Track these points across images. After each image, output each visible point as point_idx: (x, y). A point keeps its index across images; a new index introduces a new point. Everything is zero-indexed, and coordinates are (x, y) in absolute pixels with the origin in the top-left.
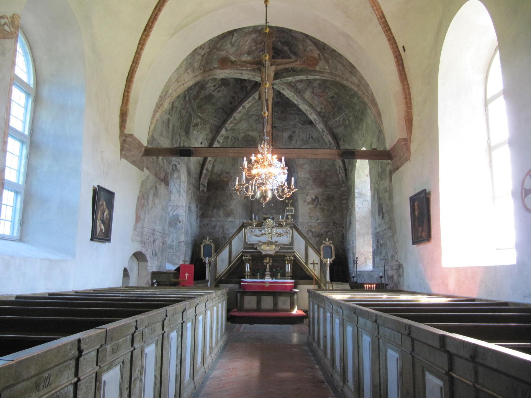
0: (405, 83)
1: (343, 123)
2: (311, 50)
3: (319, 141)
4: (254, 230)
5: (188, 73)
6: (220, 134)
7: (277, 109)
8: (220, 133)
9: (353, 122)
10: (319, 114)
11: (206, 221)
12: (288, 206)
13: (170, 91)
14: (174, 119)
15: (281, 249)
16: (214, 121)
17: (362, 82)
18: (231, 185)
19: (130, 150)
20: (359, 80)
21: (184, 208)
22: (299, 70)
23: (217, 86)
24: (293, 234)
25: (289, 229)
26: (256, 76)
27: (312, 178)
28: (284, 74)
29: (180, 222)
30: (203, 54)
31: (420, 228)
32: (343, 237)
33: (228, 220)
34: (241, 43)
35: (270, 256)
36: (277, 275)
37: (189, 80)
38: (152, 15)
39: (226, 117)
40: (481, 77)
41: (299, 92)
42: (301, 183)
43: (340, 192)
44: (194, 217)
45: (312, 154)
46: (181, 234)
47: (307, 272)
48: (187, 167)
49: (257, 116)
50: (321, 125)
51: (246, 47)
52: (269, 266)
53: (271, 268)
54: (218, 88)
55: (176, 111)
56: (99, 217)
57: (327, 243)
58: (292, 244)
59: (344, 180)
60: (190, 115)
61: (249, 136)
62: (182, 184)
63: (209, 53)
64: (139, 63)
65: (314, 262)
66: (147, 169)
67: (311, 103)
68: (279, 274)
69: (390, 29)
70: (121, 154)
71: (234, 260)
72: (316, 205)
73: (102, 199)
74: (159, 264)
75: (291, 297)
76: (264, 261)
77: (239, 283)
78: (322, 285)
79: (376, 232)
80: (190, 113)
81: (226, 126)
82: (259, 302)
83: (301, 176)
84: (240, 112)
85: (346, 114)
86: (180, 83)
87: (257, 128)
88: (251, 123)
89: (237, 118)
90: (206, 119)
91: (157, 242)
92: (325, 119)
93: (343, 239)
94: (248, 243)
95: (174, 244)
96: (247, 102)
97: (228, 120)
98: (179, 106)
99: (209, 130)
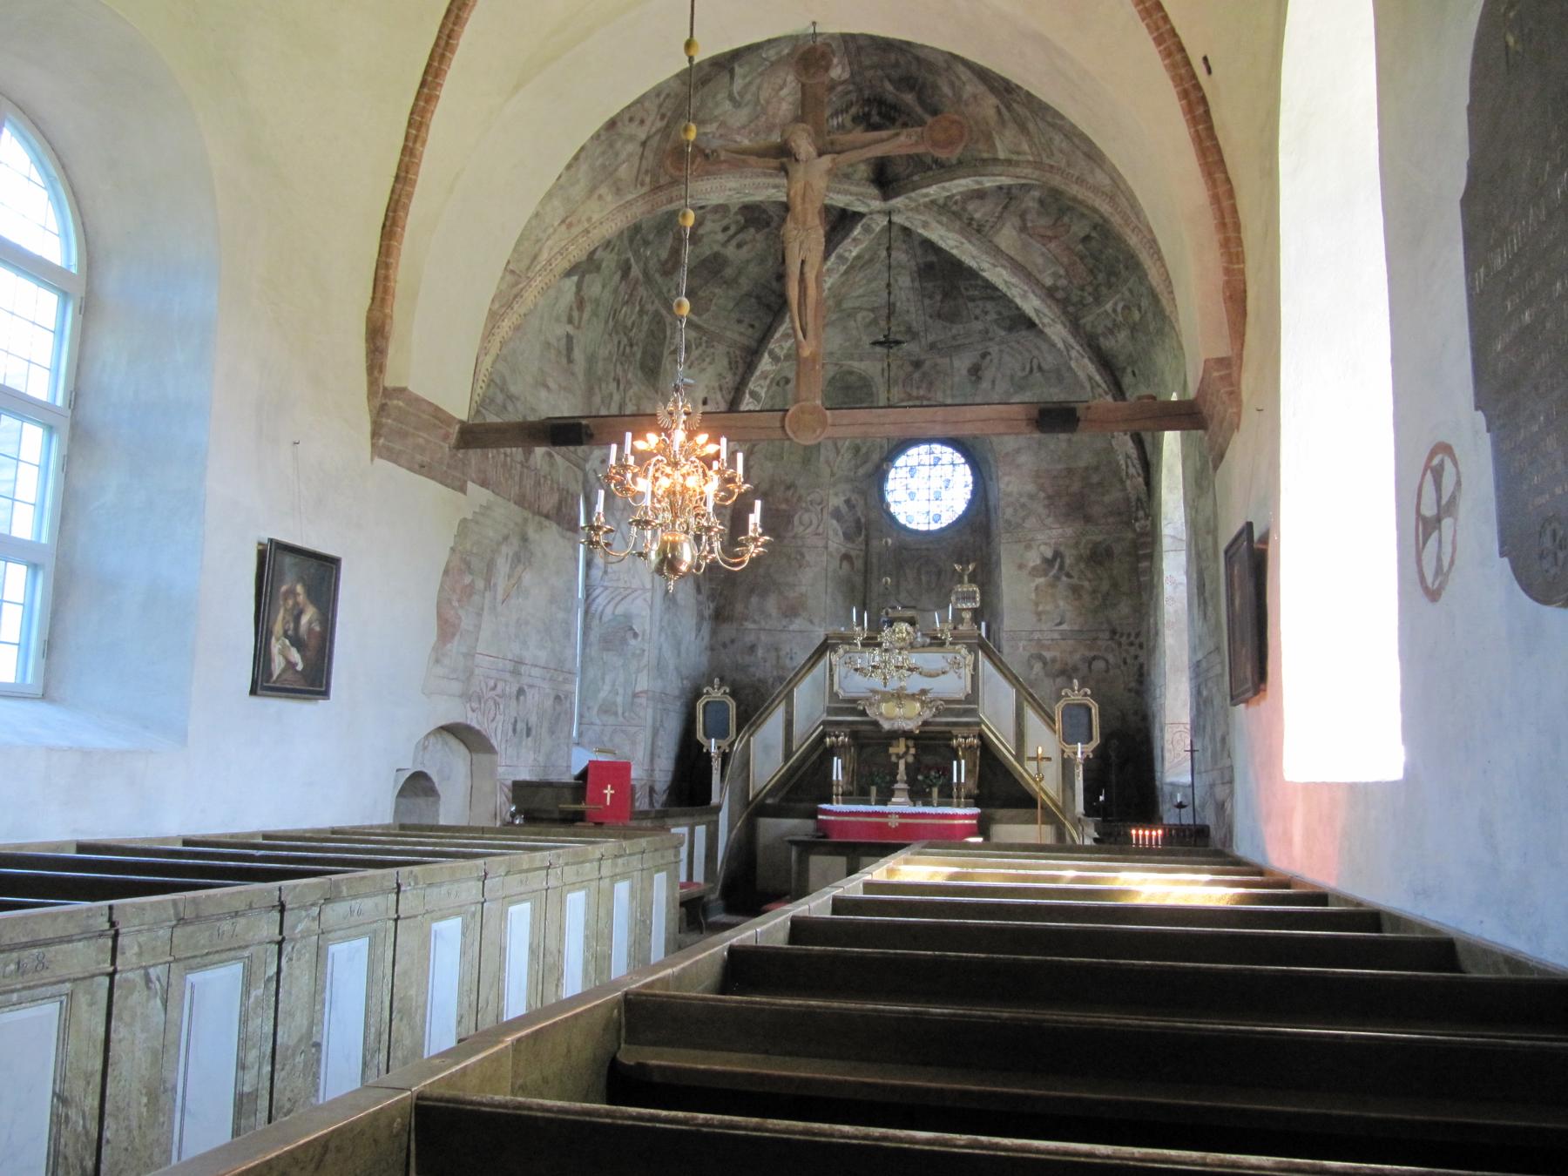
0: (1219, 176)
1: (1125, 318)
2: (975, 97)
3: (1060, 379)
6: (757, 373)
7: (930, 285)
9: (1150, 315)
10: (1050, 293)
11: (728, 631)
12: (961, 582)
13: (545, 256)
14: (592, 337)
15: (939, 713)
16: (737, 334)
18: (801, 523)
19: (404, 435)
21: (648, 595)
22: (954, 161)
24: (975, 668)
25: (964, 651)
27: (1042, 495)
28: (916, 178)
29: (635, 635)
30: (643, 137)
33: (791, 628)
34: (764, 95)
35: (908, 735)
36: (930, 794)
37: (606, 217)
38: (439, 38)
39: (769, 320)
41: (979, 231)
42: (1009, 511)
43: (1130, 535)
45: (945, 422)
46: (638, 671)
49: (873, 310)
50: (1059, 327)
51: (784, 106)
52: (907, 765)
54: (736, 234)
55: (595, 314)
56: (278, 628)
57: (1077, 694)
58: (973, 697)
59: (1144, 497)
61: (851, 373)
65: (1048, 757)
66: (484, 484)
67: (1019, 258)
68: (935, 791)
71: (800, 747)
72: (1057, 578)
74: (541, 759)
76: (892, 750)
77: (812, 814)
81: (771, 346)
83: (1009, 489)
85: (1131, 291)
86: (576, 230)
88: (854, 332)
91: (532, 697)
92: (1071, 309)
93: (1141, 682)
94: (842, 694)
95: (619, 699)
98: (607, 296)
99: (725, 362)
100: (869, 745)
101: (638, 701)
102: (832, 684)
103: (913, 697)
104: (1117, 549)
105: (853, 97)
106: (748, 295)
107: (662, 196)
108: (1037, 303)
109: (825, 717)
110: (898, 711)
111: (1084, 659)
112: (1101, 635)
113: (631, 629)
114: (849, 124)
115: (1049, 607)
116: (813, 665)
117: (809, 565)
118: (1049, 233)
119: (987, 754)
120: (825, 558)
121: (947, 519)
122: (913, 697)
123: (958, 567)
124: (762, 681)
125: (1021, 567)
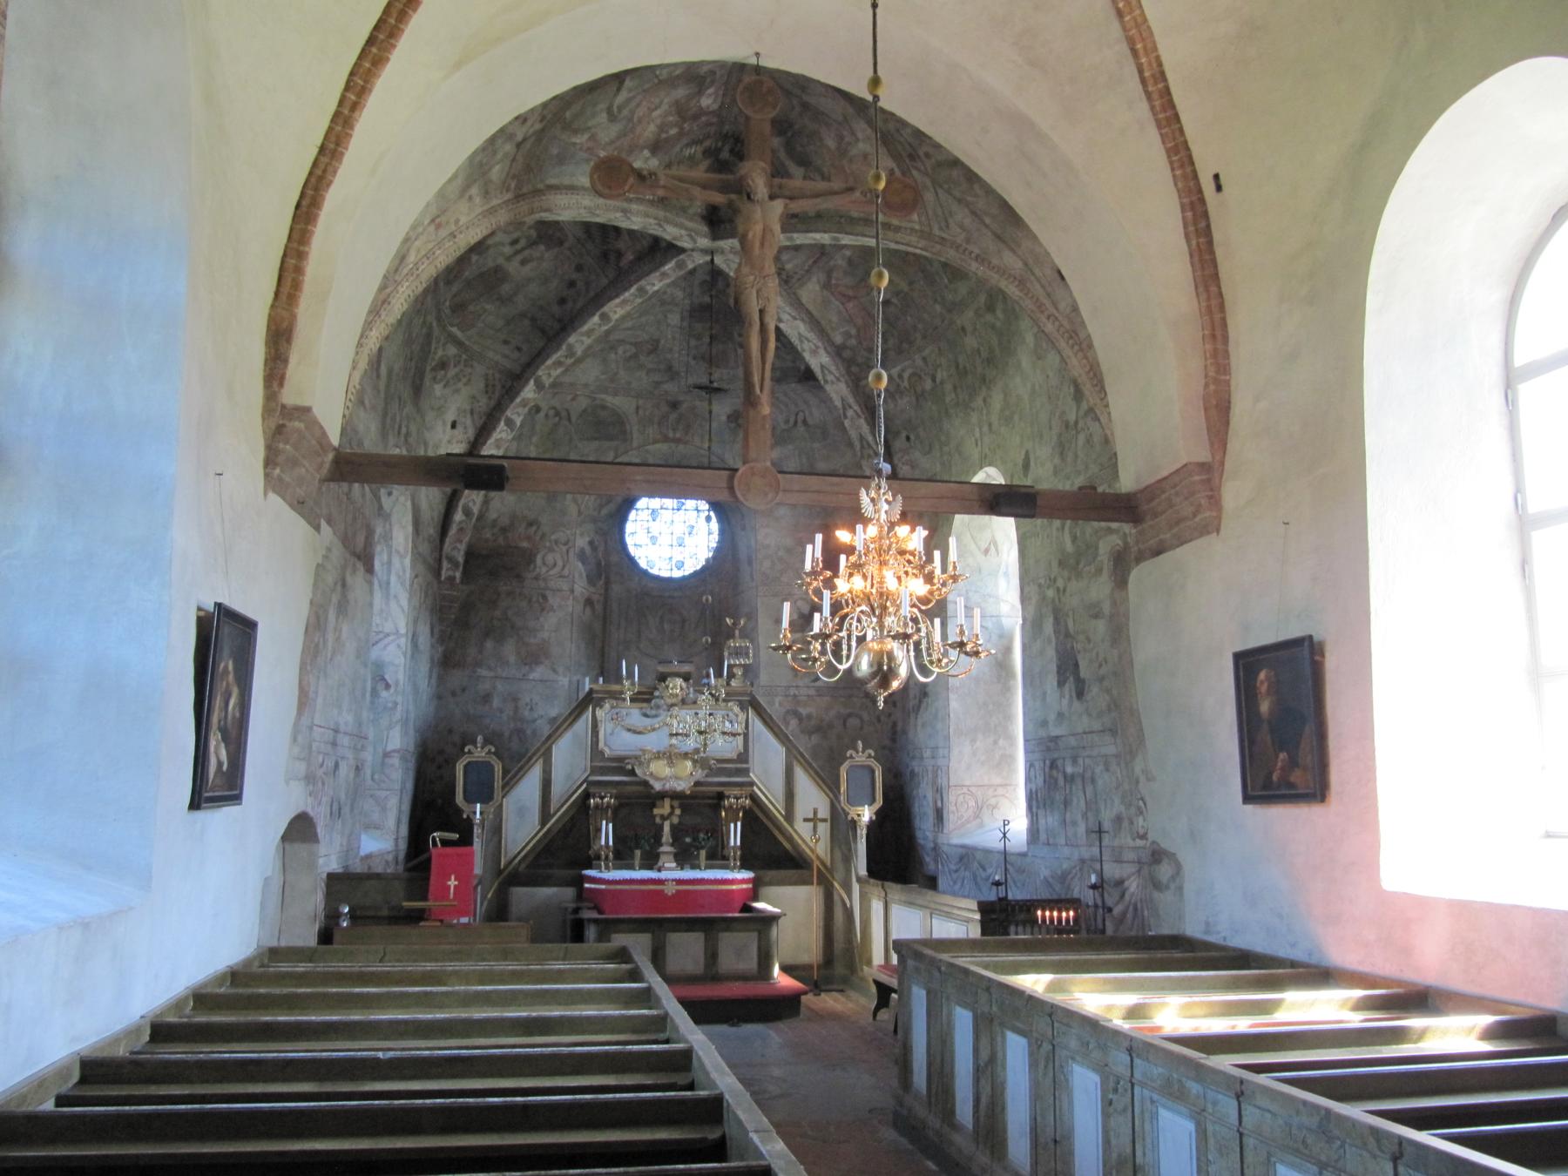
0: (1213, 289)
4: (624, 712)
5: (470, 198)
6: (518, 400)
7: (698, 326)
8: (518, 393)
9: (948, 387)
10: (838, 351)
11: (457, 678)
12: (733, 636)
13: (412, 258)
16: (500, 356)
17: (1037, 271)
20: (1026, 264)
21: (403, 640)
23: (523, 243)
25: (736, 709)
26: (668, 221)
29: (388, 686)
30: (519, 137)
31: (1283, 756)
34: (640, 112)
35: (675, 796)
36: (697, 857)
37: (471, 224)
39: (541, 344)
40: (1495, 297)
41: (786, 282)
42: (767, 564)
44: (424, 667)
46: (390, 727)
47: (787, 845)
48: (413, 504)
49: (635, 344)
52: (672, 826)
56: (215, 719)
58: (743, 757)
60: (429, 335)
61: (604, 407)
62: (396, 561)
63: (540, 135)
64: (342, 154)
66: (329, 522)
68: (703, 853)
69: (1177, 117)
70: (266, 475)
71: (559, 813)
73: (226, 652)
76: (656, 811)
79: (1042, 733)
80: (430, 327)
81: (540, 373)
84: (589, 333)
85: (924, 359)
86: (443, 233)
87: (629, 383)
88: (613, 366)
89: (579, 351)
90: (475, 347)
91: (344, 769)
93: (894, 740)
94: (607, 752)
96: (617, 301)
97: (548, 356)
99: (482, 385)
101: (389, 761)
103: (686, 756)
105: (713, 129)
106: (523, 315)
107: (524, 206)
108: (825, 359)
110: (667, 771)
113: (383, 679)
114: (699, 155)
116: (575, 720)
117: (552, 609)
118: (851, 293)
119: (756, 820)
120: (570, 602)
121: (688, 570)
122: (686, 756)
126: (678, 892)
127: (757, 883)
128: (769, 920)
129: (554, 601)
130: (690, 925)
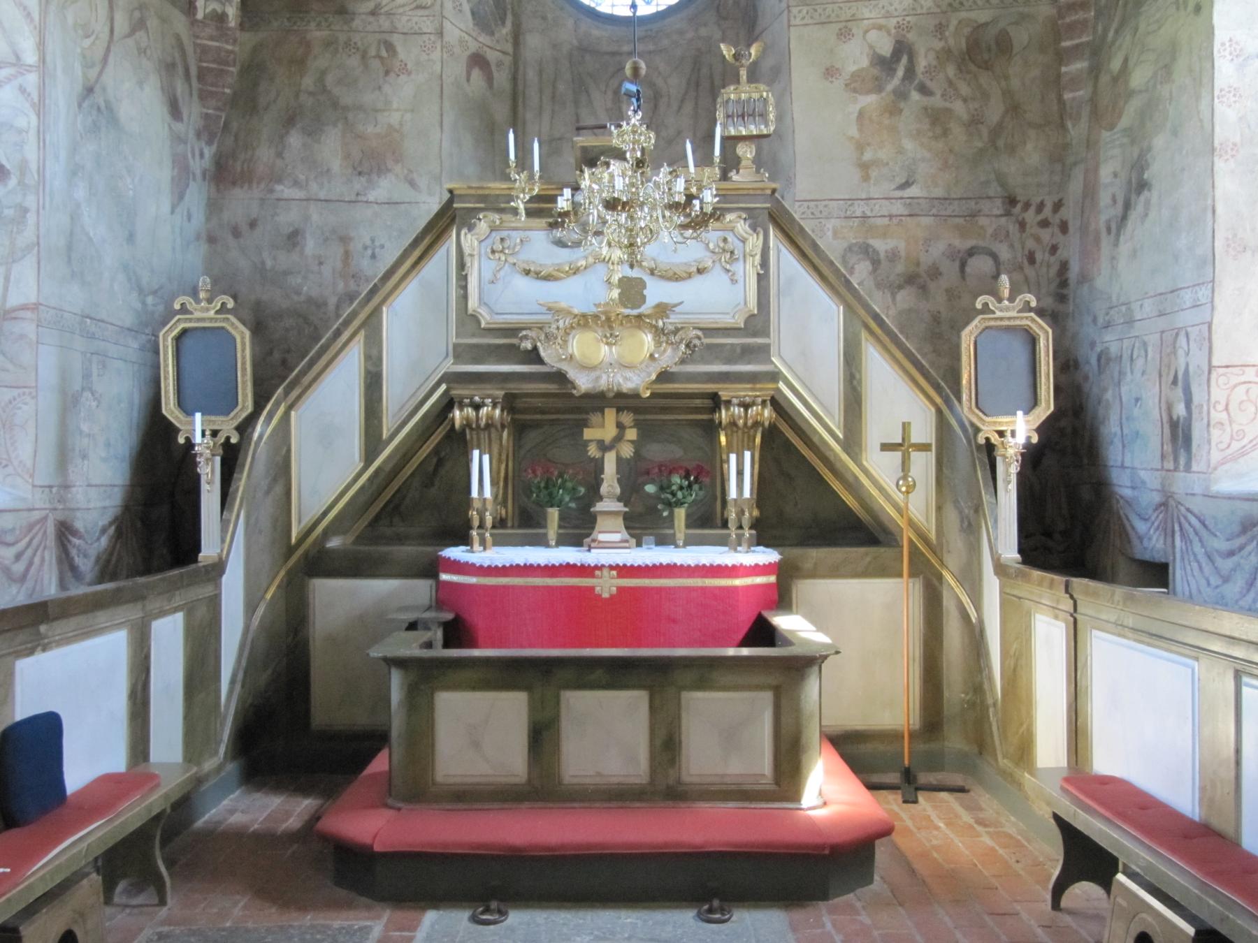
4: (516, 236)
11: (241, 202)
15: (692, 352)
21: (32, 79)
24: (765, 263)
25: (742, 227)
32: (1064, 283)
35: (623, 401)
36: (670, 520)
52: (619, 460)
53: (632, 476)
58: (758, 323)
68: (681, 514)
72: (901, 95)
75: (777, 691)
76: (588, 434)
78: (948, 577)
82: (542, 736)
93: (1062, 298)
94: (486, 319)
100: (537, 425)
102: (464, 297)
104: (1020, 36)
109: (449, 366)
111: (952, 254)
112: (985, 206)
115: (883, 154)
117: (404, 69)
119: (784, 447)
120: (436, 55)
123: (727, 51)
124: (320, 304)
125: (830, 72)
126: (621, 590)
127: (786, 574)
128: (801, 665)
129: (406, 52)
130: (618, 673)
